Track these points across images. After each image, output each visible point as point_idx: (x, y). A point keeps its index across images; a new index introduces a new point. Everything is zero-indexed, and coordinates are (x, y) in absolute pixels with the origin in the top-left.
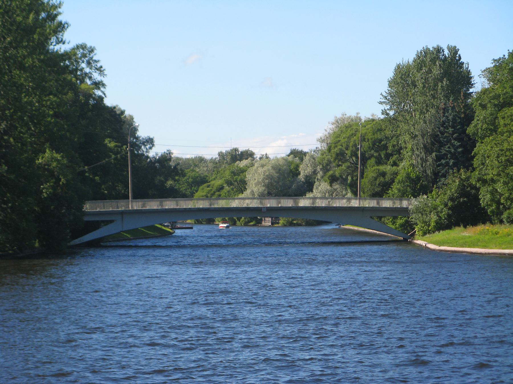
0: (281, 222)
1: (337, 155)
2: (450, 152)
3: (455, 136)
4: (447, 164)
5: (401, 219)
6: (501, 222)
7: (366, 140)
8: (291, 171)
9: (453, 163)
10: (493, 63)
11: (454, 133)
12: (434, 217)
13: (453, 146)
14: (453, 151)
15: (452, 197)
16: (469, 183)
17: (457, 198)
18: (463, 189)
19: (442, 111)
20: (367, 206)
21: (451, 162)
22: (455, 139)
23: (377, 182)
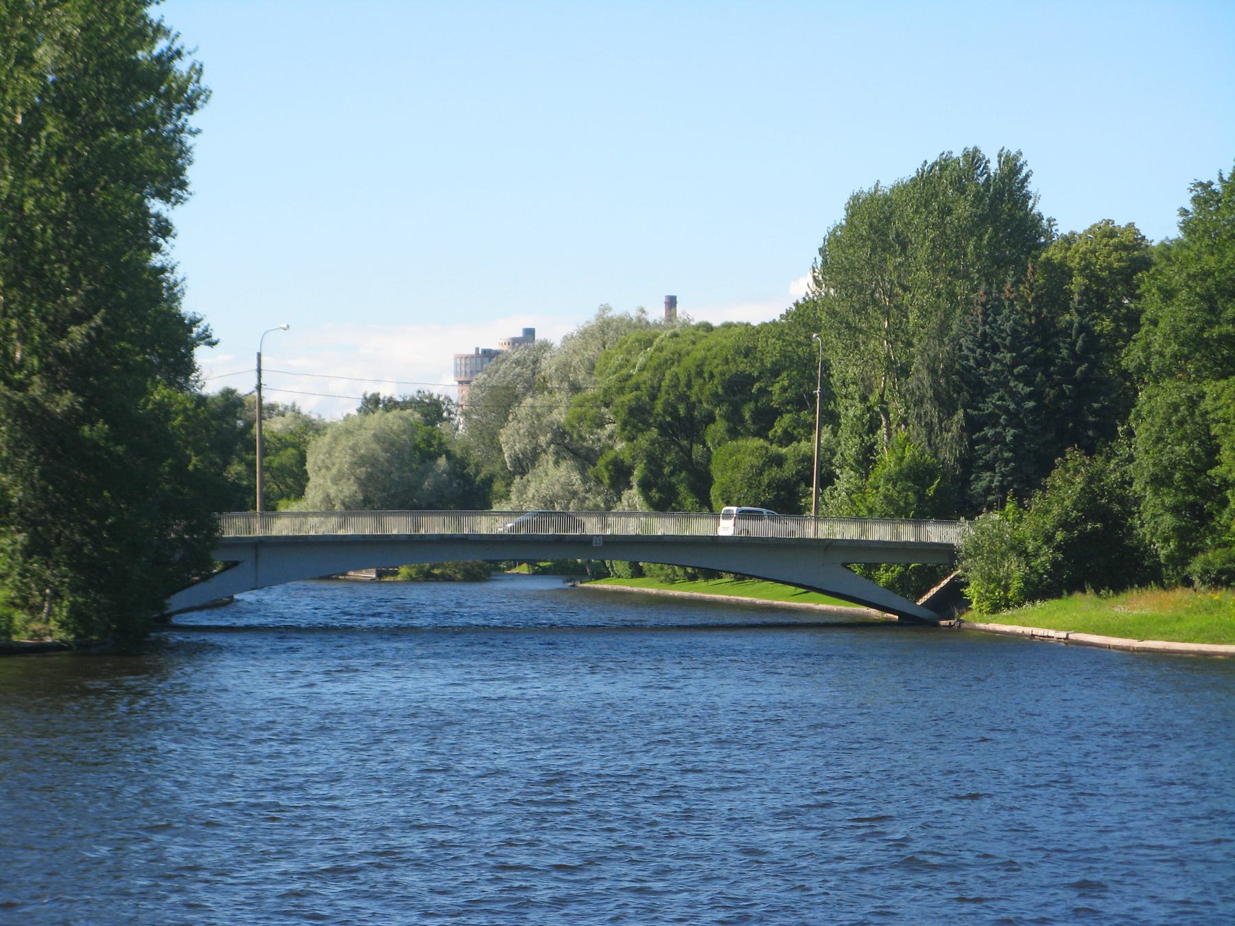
0: (404, 571)
1: (632, 412)
2: (1006, 410)
3: (1018, 370)
4: (999, 439)
5: (887, 571)
6: (1187, 582)
7: (706, 375)
8: (416, 447)
9: (1015, 436)
10: (1191, 191)
11: (1015, 364)
12: (1015, 570)
13: (1013, 394)
14: (1012, 406)
15: (1065, 520)
16: (1103, 486)
17: (1078, 522)
18: (1093, 500)
19: (979, 309)
20: (839, 537)
21: (1010, 434)
22: (1018, 378)
23: (765, 479)
